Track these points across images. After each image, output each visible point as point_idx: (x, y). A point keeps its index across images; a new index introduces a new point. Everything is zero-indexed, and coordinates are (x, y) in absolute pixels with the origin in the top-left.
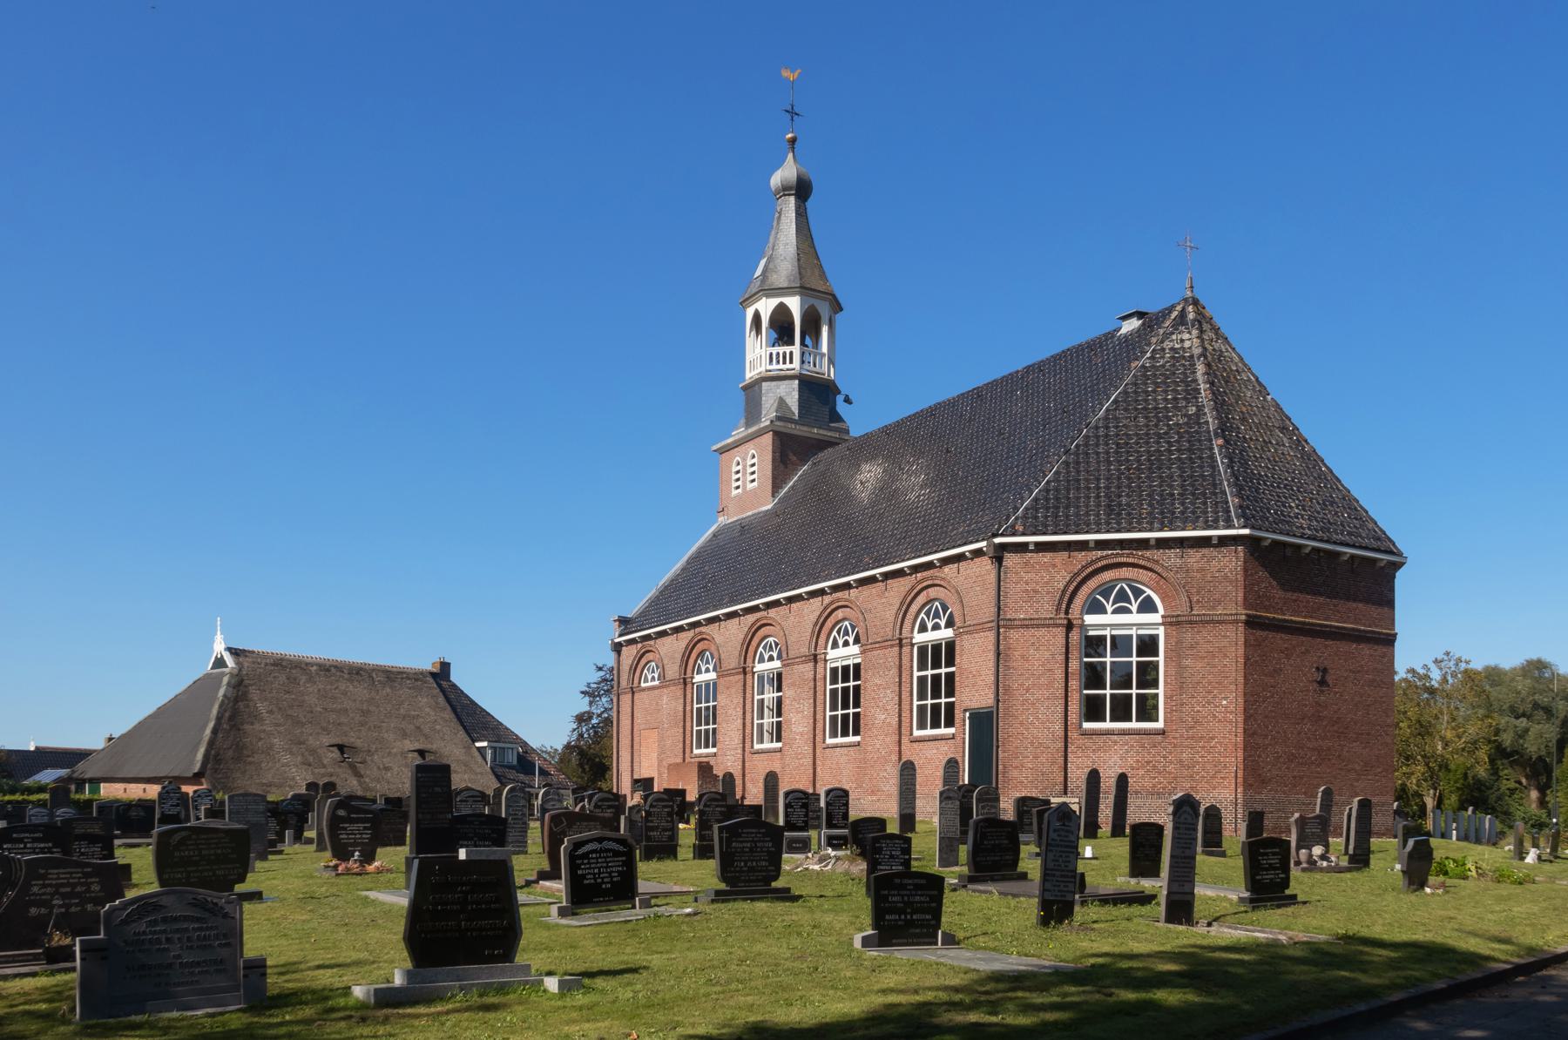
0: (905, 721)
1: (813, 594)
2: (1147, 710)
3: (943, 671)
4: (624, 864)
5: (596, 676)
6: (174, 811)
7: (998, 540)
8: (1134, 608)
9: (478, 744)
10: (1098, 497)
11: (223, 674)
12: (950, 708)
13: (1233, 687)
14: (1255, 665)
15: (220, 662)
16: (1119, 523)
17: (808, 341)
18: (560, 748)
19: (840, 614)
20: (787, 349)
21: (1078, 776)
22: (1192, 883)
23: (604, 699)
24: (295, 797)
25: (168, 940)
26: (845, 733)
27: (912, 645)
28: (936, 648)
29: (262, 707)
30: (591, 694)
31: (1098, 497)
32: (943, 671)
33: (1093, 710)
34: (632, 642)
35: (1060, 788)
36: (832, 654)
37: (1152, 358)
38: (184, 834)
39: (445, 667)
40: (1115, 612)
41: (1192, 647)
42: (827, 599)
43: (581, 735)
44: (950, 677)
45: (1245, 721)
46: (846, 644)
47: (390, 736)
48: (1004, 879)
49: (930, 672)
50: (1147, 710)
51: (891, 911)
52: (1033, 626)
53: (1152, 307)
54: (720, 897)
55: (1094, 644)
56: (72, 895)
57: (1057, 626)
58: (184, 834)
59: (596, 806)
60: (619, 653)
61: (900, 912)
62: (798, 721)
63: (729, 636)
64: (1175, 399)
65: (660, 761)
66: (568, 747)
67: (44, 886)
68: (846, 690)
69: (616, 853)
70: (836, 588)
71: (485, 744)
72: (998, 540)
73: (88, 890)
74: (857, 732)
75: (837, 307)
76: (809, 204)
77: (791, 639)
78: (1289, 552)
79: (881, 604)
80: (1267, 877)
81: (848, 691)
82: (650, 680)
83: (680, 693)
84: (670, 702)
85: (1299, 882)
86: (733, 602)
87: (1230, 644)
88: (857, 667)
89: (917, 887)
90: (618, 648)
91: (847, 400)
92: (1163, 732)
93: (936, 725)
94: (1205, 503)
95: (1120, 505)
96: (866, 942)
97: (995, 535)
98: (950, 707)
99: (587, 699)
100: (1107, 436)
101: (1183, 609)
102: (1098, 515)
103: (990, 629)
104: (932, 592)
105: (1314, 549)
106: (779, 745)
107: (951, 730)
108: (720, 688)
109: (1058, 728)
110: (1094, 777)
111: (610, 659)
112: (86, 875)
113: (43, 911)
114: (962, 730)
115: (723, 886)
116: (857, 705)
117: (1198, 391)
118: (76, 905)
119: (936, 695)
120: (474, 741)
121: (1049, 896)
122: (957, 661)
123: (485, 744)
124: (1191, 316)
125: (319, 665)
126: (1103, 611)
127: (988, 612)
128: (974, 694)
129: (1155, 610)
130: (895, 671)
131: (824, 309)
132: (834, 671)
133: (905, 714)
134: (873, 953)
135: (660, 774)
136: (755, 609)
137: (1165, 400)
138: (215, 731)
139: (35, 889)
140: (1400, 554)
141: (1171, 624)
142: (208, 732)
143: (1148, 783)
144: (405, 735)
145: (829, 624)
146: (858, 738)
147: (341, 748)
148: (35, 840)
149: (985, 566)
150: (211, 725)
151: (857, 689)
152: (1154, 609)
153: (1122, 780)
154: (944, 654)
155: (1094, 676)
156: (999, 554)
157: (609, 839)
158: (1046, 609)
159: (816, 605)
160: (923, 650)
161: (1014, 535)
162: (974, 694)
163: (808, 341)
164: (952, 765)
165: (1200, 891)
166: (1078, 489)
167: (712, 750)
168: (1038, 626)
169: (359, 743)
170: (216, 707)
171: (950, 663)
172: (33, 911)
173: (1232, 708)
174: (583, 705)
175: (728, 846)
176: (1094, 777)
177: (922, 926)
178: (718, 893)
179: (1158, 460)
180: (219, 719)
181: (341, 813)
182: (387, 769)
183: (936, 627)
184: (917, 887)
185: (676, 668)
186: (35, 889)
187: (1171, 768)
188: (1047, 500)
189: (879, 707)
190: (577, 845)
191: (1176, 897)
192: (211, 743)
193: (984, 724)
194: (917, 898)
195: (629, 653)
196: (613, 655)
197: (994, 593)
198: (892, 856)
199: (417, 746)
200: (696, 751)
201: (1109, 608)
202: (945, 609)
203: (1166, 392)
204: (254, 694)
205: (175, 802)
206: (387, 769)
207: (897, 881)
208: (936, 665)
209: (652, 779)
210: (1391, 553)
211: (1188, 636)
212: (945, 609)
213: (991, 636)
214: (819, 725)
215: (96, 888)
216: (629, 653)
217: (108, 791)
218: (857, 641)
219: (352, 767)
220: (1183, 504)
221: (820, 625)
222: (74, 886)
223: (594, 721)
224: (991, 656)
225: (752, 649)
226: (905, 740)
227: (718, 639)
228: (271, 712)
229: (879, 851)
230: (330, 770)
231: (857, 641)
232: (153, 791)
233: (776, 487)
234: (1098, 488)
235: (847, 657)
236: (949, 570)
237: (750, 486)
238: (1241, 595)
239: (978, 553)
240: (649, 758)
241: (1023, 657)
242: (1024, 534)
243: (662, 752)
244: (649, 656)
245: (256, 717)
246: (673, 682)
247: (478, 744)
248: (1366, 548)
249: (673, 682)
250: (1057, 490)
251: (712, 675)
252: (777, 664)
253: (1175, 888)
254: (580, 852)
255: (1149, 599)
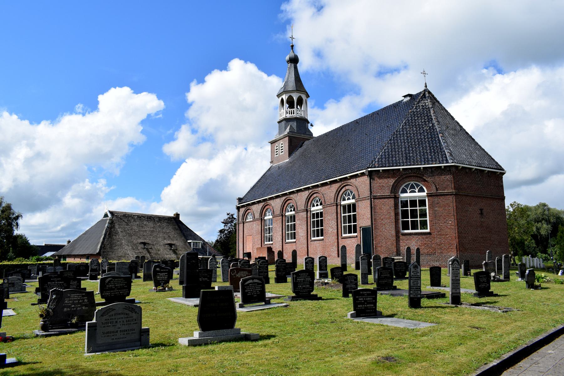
0: (339, 231)
1: (306, 189)
2: (424, 225)
3: (352, 214)
4: (261, 287)
5: (226, 217)
6: (95, 267)
7: (369, 169)
8: (417, 191)
9: (189, 241)
10: (402, 154)
11: (107, 219)
12: (355, 226)
13: (453, 217)
14: (459, 210)
15: (106, 215)
16: (410, 162)
17: (299, 107)
18: (214, 241)
19: (315, 195)
20: (292, 110)
21: (403, 249)
22: (459, 289)
23: (229, 225)
24: (132, 262)
25: (116, 322)
26: (318, 236)
27: (341, 205)
28: (349, 205)
29: (119, 230)
30: (225, 223)
31: (402, 154)
32: (352, 214)
33: (405, 226)
34: (243, 206)
35: (395, 253)
36: (313, 209)
37: (416, 108)
38: (110, 279)
39: (177, 215)
40: (410, 192)
41: (438, 204)
42: (310, 191)
43: (221, 237)
44: (354, 215)
45: (458, 229)
46: (317, 205)
47: (160, 239)
48: (389, 289)
49: (347, 214)
50: (424, 225)
51: (361, 303)
52: (383, 198)
53: (414, 93)
54: (293, 299)
55: (405, 204)
56: (79, 303)
57: (391, 198)
58: (110, 279)
59: (242, 265)
60: (239, 211)
61: (363, 304)
62: (301, 231)
63: (277, 204)
64: (425, 121)
65: (253, 247)
66: (217, 241)
67: (69, 300)
68: (318, 221)
69: (258, 284)
70: (313, 187)
71: (191, 241)
72: (369, 169)
73: (84, 302)
74: (322, 236)
75: (308, 96)
76: (298, 65)
77: (298, 204)
78: (467, 171)
79: (329, 192)
80: (483, 286)
81: (318, 222)
82: (250, 218)
83: (260, 223)
84: (257, 226)
85: (494, 287)
86: (277, 192)
87: (451, 201)
88: (321, 213)
89: (368, 295)
90: (238, 208)
91: (312, 125)
92: (429, 234)
93: (350, 232)
94: (438, 155)
95: (410, 156)
96: (352, 316)
97: (368, 168)
98: (355, 226)
99: (224, 225)
100: (403, 134)
101: (434, 191)
102: (403, 160)
103: (368, 199)
104: (347, 187)
105: (476, 169)
106: (295, 240)
107: (356, 234)
108: (274, 221)
109: (393, 232)
110: (409, 249)
111: (234, 212)
112: (83, 296)
113: (68, 309)
114: (359, 234)
115: (294, 295)
116: (322, 226)
117: (432, 119)
118: (79, 307)
119: (350, 222)
120: (187, 240)
121: (411, 296)
122: (357, 210)
123: (191, 241)
124: (427, 95)
125: (137, 216)
126: (407, 192)
127: (367, 193)
128: (364, 221)
129: (424, 191)
130: (335, 214)
131: (304, 97)
132: (314, 214)
133: (339, 229)
134: (356, 320)
135: (253, 251)
136: (285, 194)
137: (422, 122)
138: (104, 239)
139: (66, 302)
140: (503, 170)
141: (430, 196)
142: (102, 239)
143: (426, 251)
144: (165, 239)
145: (311, 199)
146: (322, 238)
147: (144, 244)
148: (58, 281)
149: (366, 179)
150: (103, 236)
151: (322, 220)
152: (424, 191)
153: (418, 250)
154: (353, 208)
155: (405, 214)
156: (371, 175)
157: (256, 279)
158: (387, 193)
159: (307, 193)
160: (344, 206)
161: (375, 167)
162: (364, 221)
163: (299, 107)
164: (358, 246)
165: (462, 291)
166: (395, 152)
167: (271, 242)
168: (384, 198)
169: (150, 242)
170: (105, 230)
171: (354, 211)
172: (65, 309)
173: (453, 224)
174: (222, 227)
175: (296, 280)
176: (409, 249)
177: (370, 309)
178: (293, 297)
179: (421, 141)
180: (105, 235)
181: (158, 269)
182: (159, 250)
183: (349, 199)
184: (368, 295)
185: (259, 215)
186: (66, 302)
187: (433, 246)
188: (385, 155)
189: (330, 225)
190: (244, 281)
191: (454, 295)
192: (103, 243)
193: (367, 233)
194: (368, 299)
195: (242, 210)
196: (236, 211)
197: (369, 187)
198: (351, 282)
199: (169, 242)
200: (266, 243)
201: (408, 191)
202: (352, 192)
203: (421, 119)
204: (117, 226)
205: (96, 264)
206: (159, 250)
207: (361, 293)
208: (349, 212)
209: (250, 253)
210: (501, 170)
211: (436, 199)
212: (352, 192)
213: (369, 201)
214: (309, 233)
215: (86, 300)
216: (242, 210)
217: (69, 260)
218: (321, 204)
219: (147, 249)
220: (431, 155)
221: (308, 199)
222: (79, 300)
223: (226, 232)
224: (369, 208)
225: (285, 208)
226: (340, 238)
227: (273, 205)
228: (122, 232)
229: (347, 280)
230: (141, 251)
231: (321, 204)
232: (89, 261)
233: (290, 154)
234: (402, 151)
235: (318, 210)
236: (353, 181)
237: (281, 154)
238: (453, 185)
239: (363, 174)
240: (250, 245)
241: (380, 208)
242: (378, 167)
243: (254, 243)
244: (249, 211)
245: (117, 233)
246: (257, 220)
247: (189, 241)
248: (492, 168)
249: (257, 220)
250: (388, 152)
251: (271, 217)
252: (293, 213)
253: (454, 291)
254: (246, 283)
255: (421, 187)
